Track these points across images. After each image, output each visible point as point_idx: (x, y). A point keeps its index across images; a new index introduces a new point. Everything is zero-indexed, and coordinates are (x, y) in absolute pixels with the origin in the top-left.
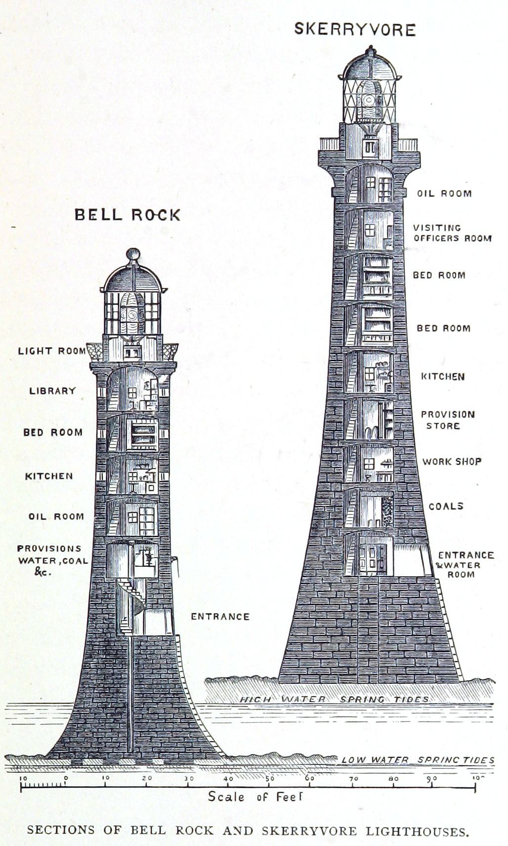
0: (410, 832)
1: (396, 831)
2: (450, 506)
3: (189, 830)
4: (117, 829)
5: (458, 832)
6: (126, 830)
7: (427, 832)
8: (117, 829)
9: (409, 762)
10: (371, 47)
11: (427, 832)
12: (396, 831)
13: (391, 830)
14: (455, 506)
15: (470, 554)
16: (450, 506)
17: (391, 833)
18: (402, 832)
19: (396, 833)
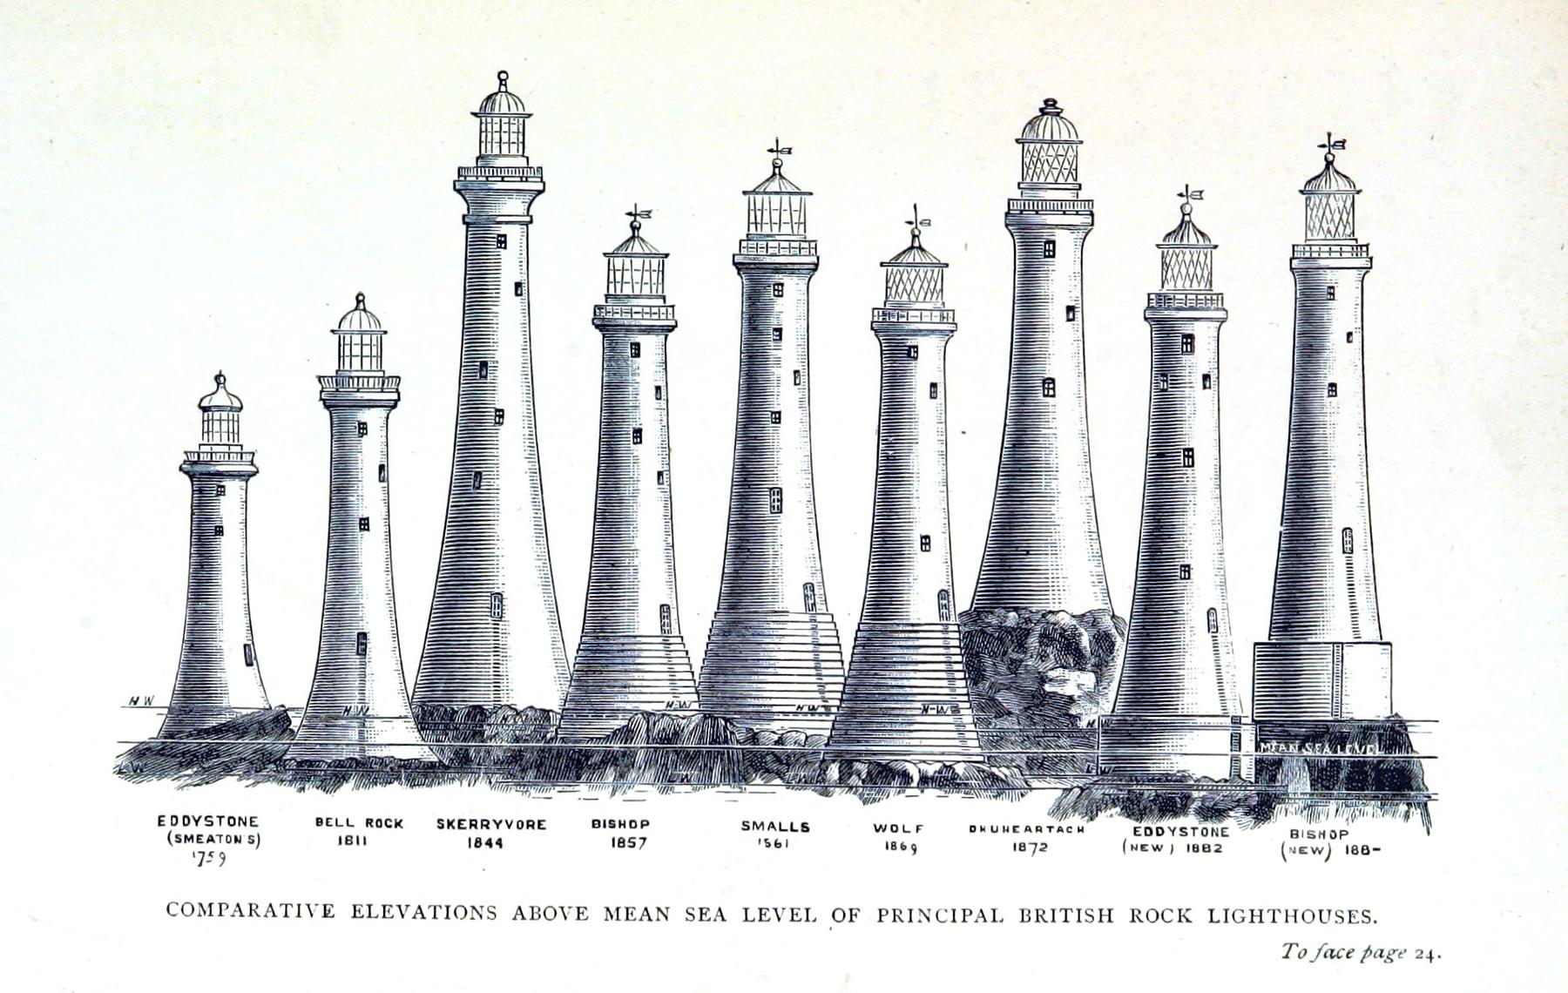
0: (1280, 917)
1: (206, 910)
2: (989, 916)
3: (1152, 916)
4: (852, 915)
5: (1359, 917)
6: (868, 915)
7: (1308, 916)
8: (852, 915)
9: (662, 384)
10: (319, 378)
11: (1308, 916)
12: (206, 910)
13: (1248, 915)
14: (797, 826)
15: (772, 825)
16: (989, 916)
17: (1248, 918)
18: (1267, 917)
19: (1256, 919)
